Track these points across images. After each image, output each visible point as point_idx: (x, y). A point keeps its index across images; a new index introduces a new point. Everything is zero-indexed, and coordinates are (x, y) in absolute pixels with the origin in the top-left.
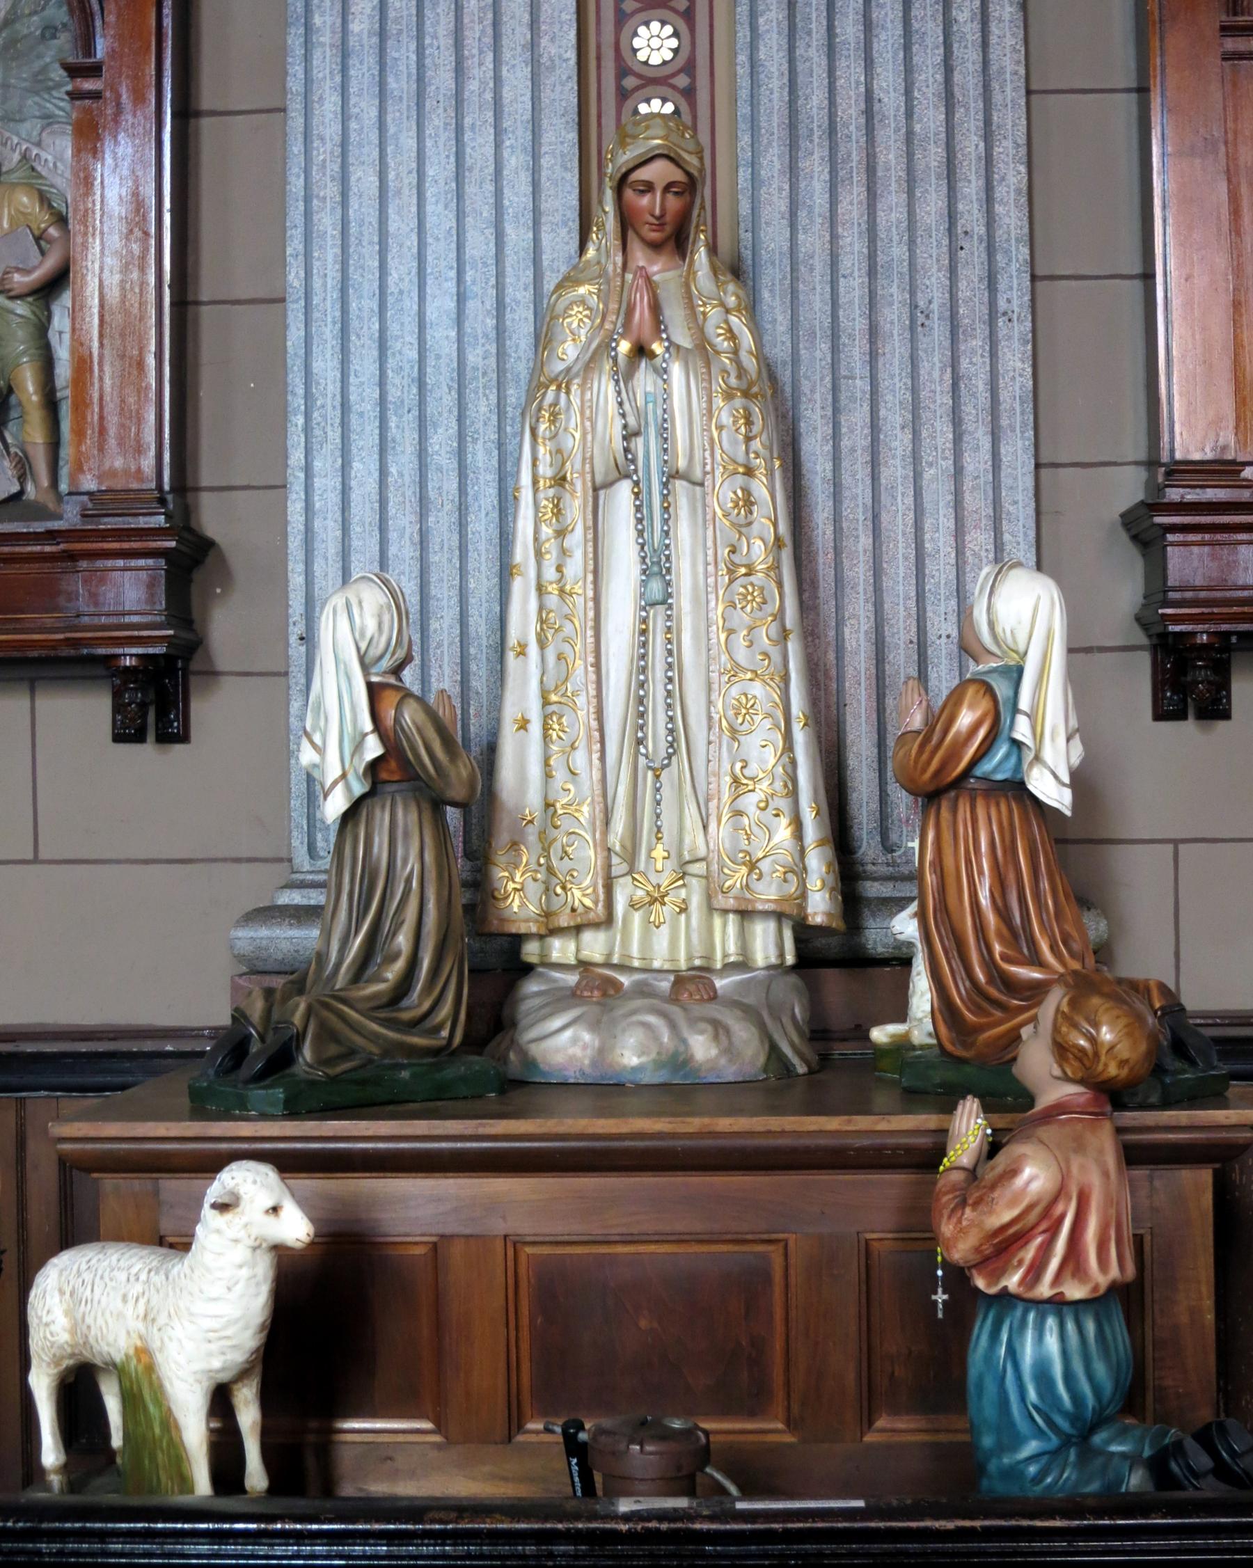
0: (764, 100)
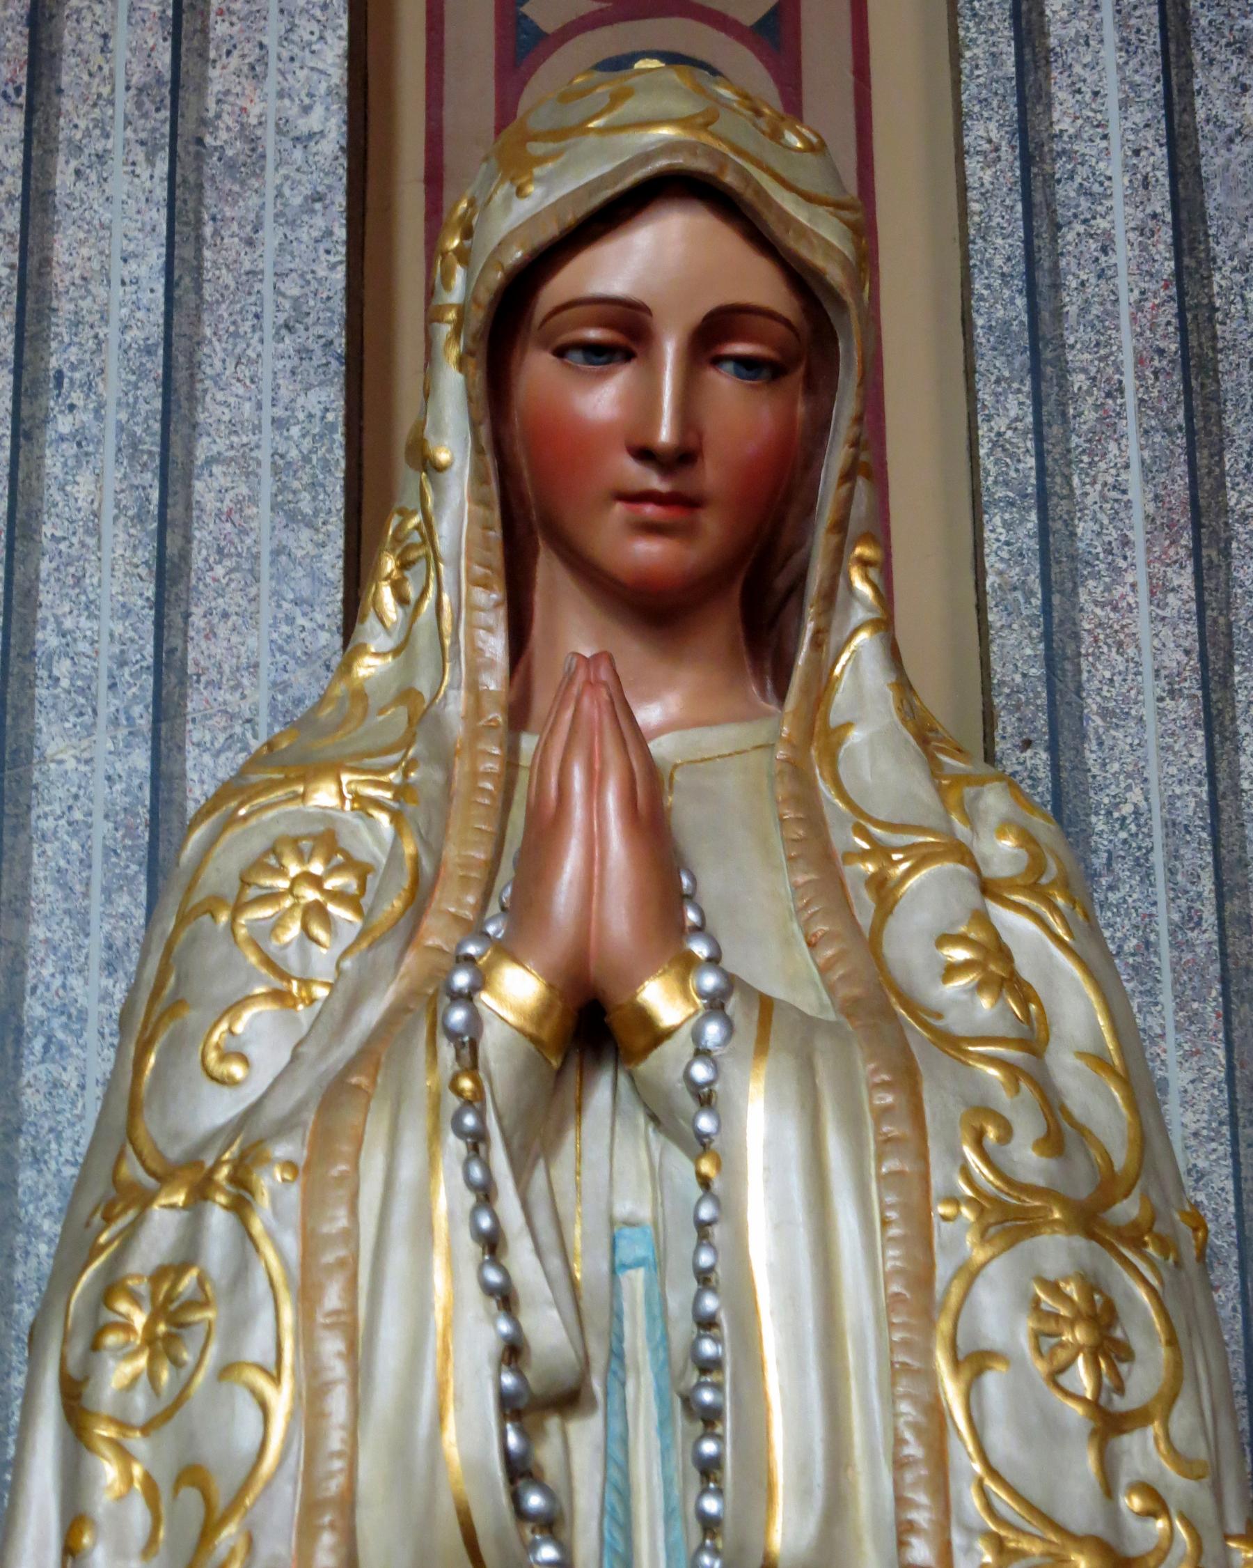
0: (1075, 273)
